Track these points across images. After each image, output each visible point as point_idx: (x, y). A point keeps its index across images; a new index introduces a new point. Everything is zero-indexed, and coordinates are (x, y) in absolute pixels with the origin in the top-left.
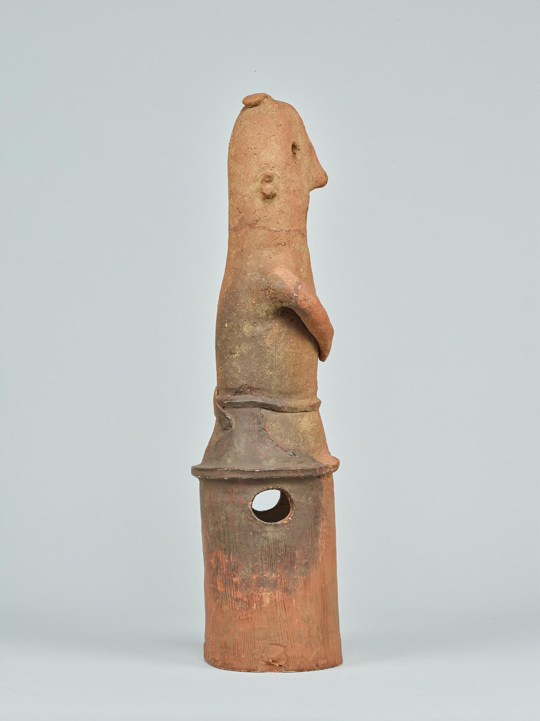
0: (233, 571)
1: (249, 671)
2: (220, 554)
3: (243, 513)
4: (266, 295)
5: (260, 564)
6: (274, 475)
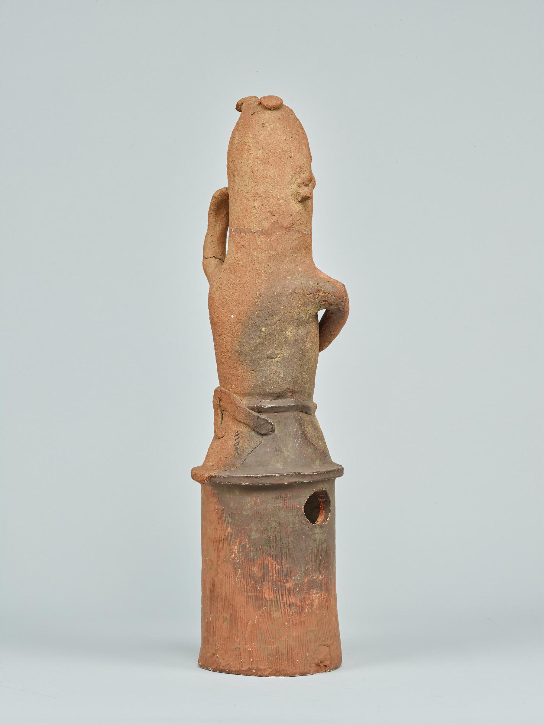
0: (285, 576)
1: (302, 674)
2: (269, 561)
3: (297, 517)
4: (314, 299)
5: (311, 567)
6: (260, 482)
